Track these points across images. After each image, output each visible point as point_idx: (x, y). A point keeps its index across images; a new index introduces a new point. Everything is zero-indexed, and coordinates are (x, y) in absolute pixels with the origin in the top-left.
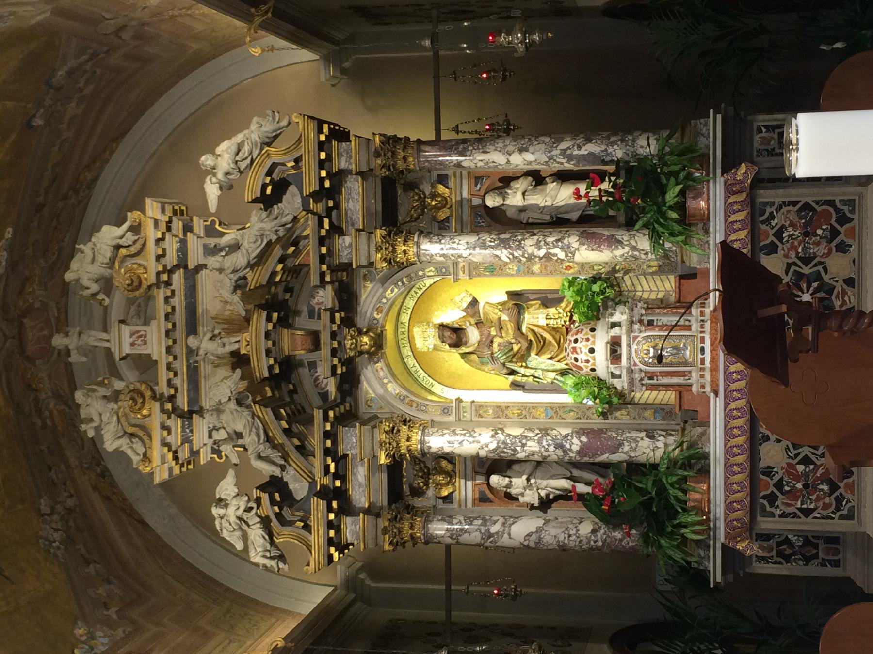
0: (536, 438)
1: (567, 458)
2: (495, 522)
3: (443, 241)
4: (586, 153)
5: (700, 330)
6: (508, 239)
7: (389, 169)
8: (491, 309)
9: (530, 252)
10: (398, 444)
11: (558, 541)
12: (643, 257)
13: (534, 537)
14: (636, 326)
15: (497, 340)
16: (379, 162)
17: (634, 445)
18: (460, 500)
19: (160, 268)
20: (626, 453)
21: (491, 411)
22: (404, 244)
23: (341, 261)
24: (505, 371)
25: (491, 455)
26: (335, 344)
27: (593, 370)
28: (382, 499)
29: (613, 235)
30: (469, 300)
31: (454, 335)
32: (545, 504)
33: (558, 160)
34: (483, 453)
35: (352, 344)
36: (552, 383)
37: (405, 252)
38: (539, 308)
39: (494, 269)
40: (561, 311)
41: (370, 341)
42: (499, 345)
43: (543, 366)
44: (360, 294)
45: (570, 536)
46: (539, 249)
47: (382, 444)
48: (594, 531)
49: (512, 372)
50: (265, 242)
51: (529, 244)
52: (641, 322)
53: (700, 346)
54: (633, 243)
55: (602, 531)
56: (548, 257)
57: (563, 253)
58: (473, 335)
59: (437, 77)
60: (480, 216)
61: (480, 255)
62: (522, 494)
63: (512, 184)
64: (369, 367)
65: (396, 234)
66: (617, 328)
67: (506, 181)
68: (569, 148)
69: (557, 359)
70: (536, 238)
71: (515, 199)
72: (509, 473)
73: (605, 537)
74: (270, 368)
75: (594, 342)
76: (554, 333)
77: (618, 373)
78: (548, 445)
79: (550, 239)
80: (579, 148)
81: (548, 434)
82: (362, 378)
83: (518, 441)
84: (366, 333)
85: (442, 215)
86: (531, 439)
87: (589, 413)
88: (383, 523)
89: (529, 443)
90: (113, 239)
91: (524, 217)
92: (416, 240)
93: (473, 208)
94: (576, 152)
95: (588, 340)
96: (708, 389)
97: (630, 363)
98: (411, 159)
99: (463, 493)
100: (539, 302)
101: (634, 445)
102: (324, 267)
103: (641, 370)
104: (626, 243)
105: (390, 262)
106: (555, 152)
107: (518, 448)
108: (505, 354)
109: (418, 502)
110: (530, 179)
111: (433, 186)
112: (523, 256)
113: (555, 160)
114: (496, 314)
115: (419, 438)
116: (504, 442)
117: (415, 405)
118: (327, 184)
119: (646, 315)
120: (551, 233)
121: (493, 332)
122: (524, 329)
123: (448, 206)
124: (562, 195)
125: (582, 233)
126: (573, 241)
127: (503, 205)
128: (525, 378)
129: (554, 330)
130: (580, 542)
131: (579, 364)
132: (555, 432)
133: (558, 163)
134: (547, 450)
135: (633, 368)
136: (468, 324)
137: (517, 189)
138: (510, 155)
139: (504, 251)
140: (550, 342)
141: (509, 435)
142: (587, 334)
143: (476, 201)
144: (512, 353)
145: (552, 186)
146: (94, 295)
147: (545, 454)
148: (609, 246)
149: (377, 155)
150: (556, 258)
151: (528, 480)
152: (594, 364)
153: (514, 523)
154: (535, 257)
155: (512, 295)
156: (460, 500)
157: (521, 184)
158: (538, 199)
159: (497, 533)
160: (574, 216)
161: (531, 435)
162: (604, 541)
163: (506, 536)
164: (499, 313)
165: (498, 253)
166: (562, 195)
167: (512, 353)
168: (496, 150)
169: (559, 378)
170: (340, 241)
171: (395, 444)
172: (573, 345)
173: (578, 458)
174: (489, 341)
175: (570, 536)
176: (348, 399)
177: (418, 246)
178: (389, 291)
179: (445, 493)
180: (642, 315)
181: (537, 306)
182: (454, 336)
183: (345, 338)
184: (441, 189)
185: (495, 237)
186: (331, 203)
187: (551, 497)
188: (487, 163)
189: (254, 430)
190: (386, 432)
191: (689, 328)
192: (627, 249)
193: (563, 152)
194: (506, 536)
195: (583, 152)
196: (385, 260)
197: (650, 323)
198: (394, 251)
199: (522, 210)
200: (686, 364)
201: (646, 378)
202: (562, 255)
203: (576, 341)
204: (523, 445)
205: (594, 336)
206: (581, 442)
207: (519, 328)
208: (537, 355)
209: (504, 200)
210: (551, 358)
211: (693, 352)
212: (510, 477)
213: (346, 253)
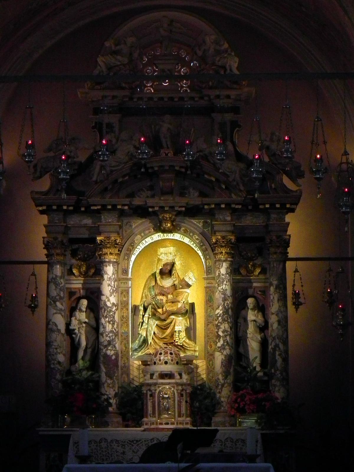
0: (113, 329)
1: (102, 348)
2: (62, 304)
3: (227, 275)
4: (277, 359)
5: (179, 422)
6: (228, 314)
7: (270, 243)
8: (185, 297)
9: (221, 326)
10: (109, 247)
11: (53, 342)
12: (218, 391)
13: (55, 328)
14: (180, 388)
15: (164, 299)
16: (274, 238)
17: (111, 386)
18: (70, 280)
19: (212, 97)
20: (106, 381)
21: (125, 299)
22: (226, 252)
23: (216, 215)
24: (146, 304)
25: (103, 303)
26: (166, 209)
27: (155, 363)
28: (73, 235)
29: (230, 374)
30: (190, 283)
31: (168, 271)
32: (70, 332)
33: (273, 342)
34: (103, 298)
35: (167, 218)
36: (139, 334)
37: (222, 253)
38: (185, 326)
39: (209, 301)
40: (184, 339)
41: (168, 228)
42: (162, 300)
43: (150, 328)
44: (196, 219)
45: (56, 349)
46: (223, 332)
47: (109, 238)
48: (59, 363)
49: (145, 309)
50: (228, 173)
51: (225, 326)
52: (182, 390)
53: (169, 422)
54: (226, 385)
55: (59, 367)
56: (219, 336)
57: (220, 346)
58: (167, 283)
59: (329, 259)
60: (242, 294)
61: (218, 296)
62: (76, 319)
63: (260, 313)
64: (151, 224)
65: (232, 247)
66: (179, 377)
67: (261, 308)
68: (279, 349)
69: (154, 337)
70: (229, 330)
71: (252, 316)
72: (88, 310)
73: (56, 369)
74: (152, 168)
75: (171, 364)
76: (170, 335)
77: (154, 377)
78: (110, 337)
79: (228, 338)
80: (280, 355)
81: (115, 337)
82: (144, 220)
83: (112, 319)
84: (172, 225)
85: (243, 271)
86: (113, 326)
87: (125, 358)
88: (60, 237)
89: (110, 326)
90: (230, 66)
91: (241, 320)
92: (228, 259)
93: (247, 289)
94: (277, 353)
95: (172, 360)
96: (146, 427)
97: (160, 384)
98: (275, 256)
99: (75, 282)
100: (189, 326)
101: (111, 386)
102: (213, 206)
103: (156, 390)
104: (226, 381)
105: (215, 243)
106: (277, 341)
107: (107, 319)
108: (156, 304)
109: (68, 253)
110: (263, 324)
111: (260, 266)
112: (219, 322)
113: (273, 341)
114: (182, 300)
115: (112, 260)
116: (111, 311)
117: (128, 252)
118: (261, 207)
119: (186, 393)
120: (232, 338)
121: (170, 296)
122: (172, 317)
123: (248, 274)
124: (253, 345)
125: (232, 356)
126: (227, 351)
127: (248, 308)
128: (141, 317)
129: (172, 335)
130: (53, 355)
131: (158, 355)
132: (117, 340)
133: (272, 342)
134: (107, 336)
135: (157, 386)
136: (174, 279)
137: (257, 317)
138: (277, 315)
139: (222, 311)
140: (164, 333)
141: (115, 313)
142: (175, 360)
143: (251, 291)
144: (157, 308)
145: (259, 337)
146: (196, 54)
147: (104, 335)
148: (224, 372)
149: (278, 237)
150: (217, 341)
151: (85, 323)
152: (158, 364)
153: (62, 315)
154: (218, 330)
155: (192, 305)
156: (70, 280)
157: (260, 318)
158: (251, 329)
159: (56, 306)
160: (241, 350)
161: (115, 326)
162: (54, 368)
163: (55, 311)
164: (182, 302)
165: (221, 308)
166: (253, 345)
167: (157, 308)
168: (279, 306)
169: (142, 338)
170: (228, 214)
171: (108, 246)
172: (169, 352)
173: (102, 354)
174: (164, 293)
175: (56, 349)
176: (131, 211)
177: (225, 261)
178: (197, 237)
179: (75, 271)
180: (186, 390)
181: (187, 325)
182: (167, 271)
183: (170, 213)
184: (258, 271)
185: (230, 306)
186: (250, 207)
187: (74, 336)
188: (272, 301)
189: (118, 164)
190: (115, 241)
191: (180, 416)
192: (222, 382)
193: (277, 346)
194: (55, 311)
195: (277, 357)
196: (217, 241)
197: (182, 395)
198: (222, 247)
199: (245, 320)
200: (160, 415)
201: (151, 393)
202: (219, 345)
203: (171, 354)
204: (109, 322)
205: (174, 364)
206: (112, 356)
207: (173, 314)
208: (157, 325)
209: (251, 309)
210: (154, 333)
211: (166, 418)
212: (86, 312)
213: (221, 217)
